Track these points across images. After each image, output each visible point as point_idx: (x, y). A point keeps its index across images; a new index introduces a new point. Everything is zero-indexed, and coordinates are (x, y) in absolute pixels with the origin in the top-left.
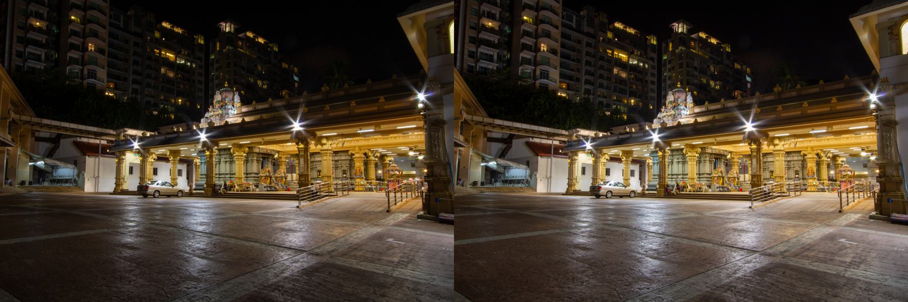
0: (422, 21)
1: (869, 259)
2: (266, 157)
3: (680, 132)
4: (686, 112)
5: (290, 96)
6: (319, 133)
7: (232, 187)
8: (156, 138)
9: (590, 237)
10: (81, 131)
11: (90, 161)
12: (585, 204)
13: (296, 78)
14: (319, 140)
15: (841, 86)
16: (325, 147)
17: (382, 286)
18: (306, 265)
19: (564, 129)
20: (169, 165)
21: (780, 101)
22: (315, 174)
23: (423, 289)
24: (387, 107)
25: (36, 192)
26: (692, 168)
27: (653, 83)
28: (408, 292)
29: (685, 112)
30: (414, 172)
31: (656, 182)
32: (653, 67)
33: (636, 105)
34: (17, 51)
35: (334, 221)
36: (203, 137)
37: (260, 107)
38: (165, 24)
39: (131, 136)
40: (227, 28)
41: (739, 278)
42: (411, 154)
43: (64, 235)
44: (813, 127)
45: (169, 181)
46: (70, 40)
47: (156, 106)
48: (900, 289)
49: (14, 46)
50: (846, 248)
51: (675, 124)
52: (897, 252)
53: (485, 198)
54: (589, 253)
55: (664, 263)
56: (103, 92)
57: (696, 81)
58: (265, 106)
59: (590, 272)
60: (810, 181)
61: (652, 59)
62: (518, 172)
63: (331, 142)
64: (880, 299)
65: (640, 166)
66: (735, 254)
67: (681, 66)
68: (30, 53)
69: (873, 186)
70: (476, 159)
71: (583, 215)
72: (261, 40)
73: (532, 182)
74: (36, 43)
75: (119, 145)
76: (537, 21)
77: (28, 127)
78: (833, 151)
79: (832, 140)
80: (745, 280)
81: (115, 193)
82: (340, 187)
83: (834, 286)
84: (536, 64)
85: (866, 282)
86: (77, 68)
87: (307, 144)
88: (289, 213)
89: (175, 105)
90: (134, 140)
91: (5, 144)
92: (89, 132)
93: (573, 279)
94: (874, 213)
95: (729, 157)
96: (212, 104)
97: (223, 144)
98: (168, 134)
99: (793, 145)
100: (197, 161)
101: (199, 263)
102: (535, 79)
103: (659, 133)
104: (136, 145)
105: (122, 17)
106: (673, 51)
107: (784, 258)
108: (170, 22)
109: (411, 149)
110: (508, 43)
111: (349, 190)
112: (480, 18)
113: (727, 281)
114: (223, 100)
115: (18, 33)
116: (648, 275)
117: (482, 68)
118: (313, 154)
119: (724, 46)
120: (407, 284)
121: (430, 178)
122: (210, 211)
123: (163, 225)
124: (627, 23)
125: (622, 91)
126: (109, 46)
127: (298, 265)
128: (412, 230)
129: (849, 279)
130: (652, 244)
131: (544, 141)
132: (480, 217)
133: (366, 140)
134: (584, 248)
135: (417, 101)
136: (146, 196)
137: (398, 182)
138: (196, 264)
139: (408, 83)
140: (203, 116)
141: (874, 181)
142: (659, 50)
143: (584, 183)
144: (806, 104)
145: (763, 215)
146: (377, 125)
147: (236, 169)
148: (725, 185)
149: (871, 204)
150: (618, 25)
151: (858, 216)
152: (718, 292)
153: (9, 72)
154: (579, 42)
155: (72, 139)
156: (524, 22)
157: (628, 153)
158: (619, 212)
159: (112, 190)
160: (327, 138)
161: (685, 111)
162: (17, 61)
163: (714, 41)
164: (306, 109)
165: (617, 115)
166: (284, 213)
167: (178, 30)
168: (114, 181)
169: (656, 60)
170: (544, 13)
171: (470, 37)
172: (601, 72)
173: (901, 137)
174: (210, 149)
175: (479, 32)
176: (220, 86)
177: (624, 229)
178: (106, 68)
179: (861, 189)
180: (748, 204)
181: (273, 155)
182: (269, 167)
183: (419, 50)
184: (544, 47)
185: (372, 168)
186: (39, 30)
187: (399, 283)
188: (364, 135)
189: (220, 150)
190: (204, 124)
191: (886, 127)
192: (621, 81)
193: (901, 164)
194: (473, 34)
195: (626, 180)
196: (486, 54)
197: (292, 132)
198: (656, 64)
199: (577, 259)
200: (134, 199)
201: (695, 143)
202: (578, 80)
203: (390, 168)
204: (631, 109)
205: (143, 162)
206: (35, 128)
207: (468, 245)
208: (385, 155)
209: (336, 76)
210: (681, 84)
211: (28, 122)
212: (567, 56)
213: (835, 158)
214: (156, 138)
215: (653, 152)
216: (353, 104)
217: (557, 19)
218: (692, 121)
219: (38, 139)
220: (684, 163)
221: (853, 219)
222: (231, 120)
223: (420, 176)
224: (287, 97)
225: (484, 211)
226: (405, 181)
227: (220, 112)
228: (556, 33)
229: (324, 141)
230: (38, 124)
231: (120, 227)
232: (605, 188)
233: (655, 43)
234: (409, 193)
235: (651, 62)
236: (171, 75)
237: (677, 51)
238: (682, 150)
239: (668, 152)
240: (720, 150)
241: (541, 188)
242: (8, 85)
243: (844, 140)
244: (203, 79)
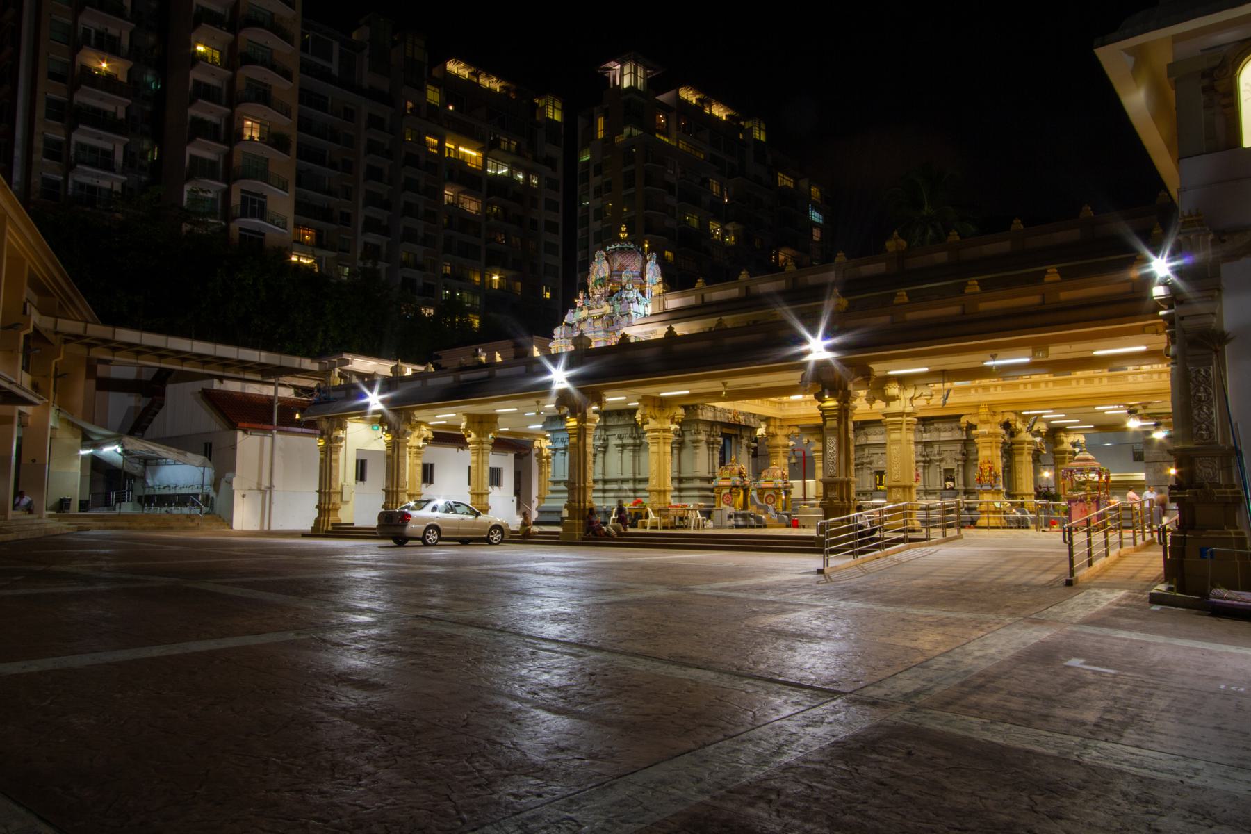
0: (1163, 58)
1: (1149, 716)
2: (732, 434)
3: (624, 363)
5: (798, 265)
6: (878, 369)
7: (639, 515)
8: (431, 382)
9: (380, 651)
10: (224, 363)
11: (248, 445)
13: (815, 216)
14: (878, 387)
16: (896, 407)
17: (1053, 789)
18: (842, 733)
20: (467, 457)
22: (868, 481)
24: (1066, 295)
25: (98, 530)
27: (552, 227)
28: (1125, 807)
29: (641, 309)
30: (1141, 476)
34: (47, 141)
35: (920, 611)
36: (559, 377)
37: (717, 295)
38: (454, 67)
40: (626, 76)
42: (1133, 424)
43: (176, 650)
45: (467, 500)
46: (192, 112)
47: (429, 292)
49: (39, 128)
52: (1225, 695)
55: (581, 725)
56: (284, 253)
58: (730, 292)
59: (378, 750)
60: (987, 498)
61: (550, 162)
62: (181, 473)
63: (912, 391)
64: (1179, 824)
65: (518, 458)
66: (778, 701)
68: (82, 147)
70: (67, 438)
72: (719, 112)
74: (99, 119)
75: (327, 401)
76: (234, 58)
77: (78, 350)
79: (1046, 386)
80: (807, 773)
82: (935, 516)
85: (1142, 780)
86: (211, 189)
87: (845, 398)
88: (797, 587)
89: (484, 289)
90: (370, 386)
91: (11, 398)
92: (245, 366)
93: (334, 767)
95: (761, 431)
96: (585, 287)
97: (614, 398)
98: (464, 369)
99: (937, 400)
100: (544, 444)
101: (547, 728)
104: (375, 400)
105: (336, 46)
108: (468, 61)
109: (1132, 412)
111: (962, 525)
112: (76, 49)
113: (757, 773)
114: (614, 277)
115: (50, 90)
118: (862, 426)
120: (1122, 785)
121: (1186, 492)
122: (579, 582)
123: (450, 622)
124: (480, 64)
126: (300, 129)
127: (820, 731)
128: (1135, 636)
133: (1009, 387)
135: (1148, 280)
136: (401, 540)
137: (1097, 502)
139: (1124, 229)
140: (558, 321)
142: (570, 136)
143: (361, 506)
146: (1037, 346)
147: (651, 466)
148: (752, 510)
152: (731, 806)
153: (25, 198)
154: (349, 115)
155: (198, 385)
157: (482, 423)
159: (308, 525)
160: (902, 381)
162: (48, 170)
166: (781, 588)
167: (492, 84)
168: (314, 499)
169: (560, 166)
171: (51, 103)
174: (577, 410)
176: (606, 238)
177: (471, 632)
178: (292, 188)
181: (753, 429)
182: (742, 462)
183: (1154, 139)
184: (251, 130)
185: (1025, 464)
186: (108, 82)
187: (1099, 780)
188: (1003, 371)
189: (605, 414)
190: (561, 342)
191: (1196, 349)
193: (1239, 453)
194: (58, 92)
197: (803, 366)
199: (345, 713)
200: (371, 549)
201: (668, 393)
202: (346, 219)
203: (1074, 465)
205: (395, 448)
206: (96, 353)
208: (1062, 429)
209: (927, 210)
211: (78, 337)
214: (431, 382)
215: (551, 419)
216: (973, 286)
219: (106, 385)
220: (638, 448)
222: (636, 332)
223: (1157, 487)
224: (791, 267)
226: (1116, 501)
229: (893, 390)
230: (105, 342)
231: (332, 628)
233: (557, 117)
234: (1127, 534)
236: (472, 206)
240: (736, 414)
242: (21, 237)
244: (559, 218)
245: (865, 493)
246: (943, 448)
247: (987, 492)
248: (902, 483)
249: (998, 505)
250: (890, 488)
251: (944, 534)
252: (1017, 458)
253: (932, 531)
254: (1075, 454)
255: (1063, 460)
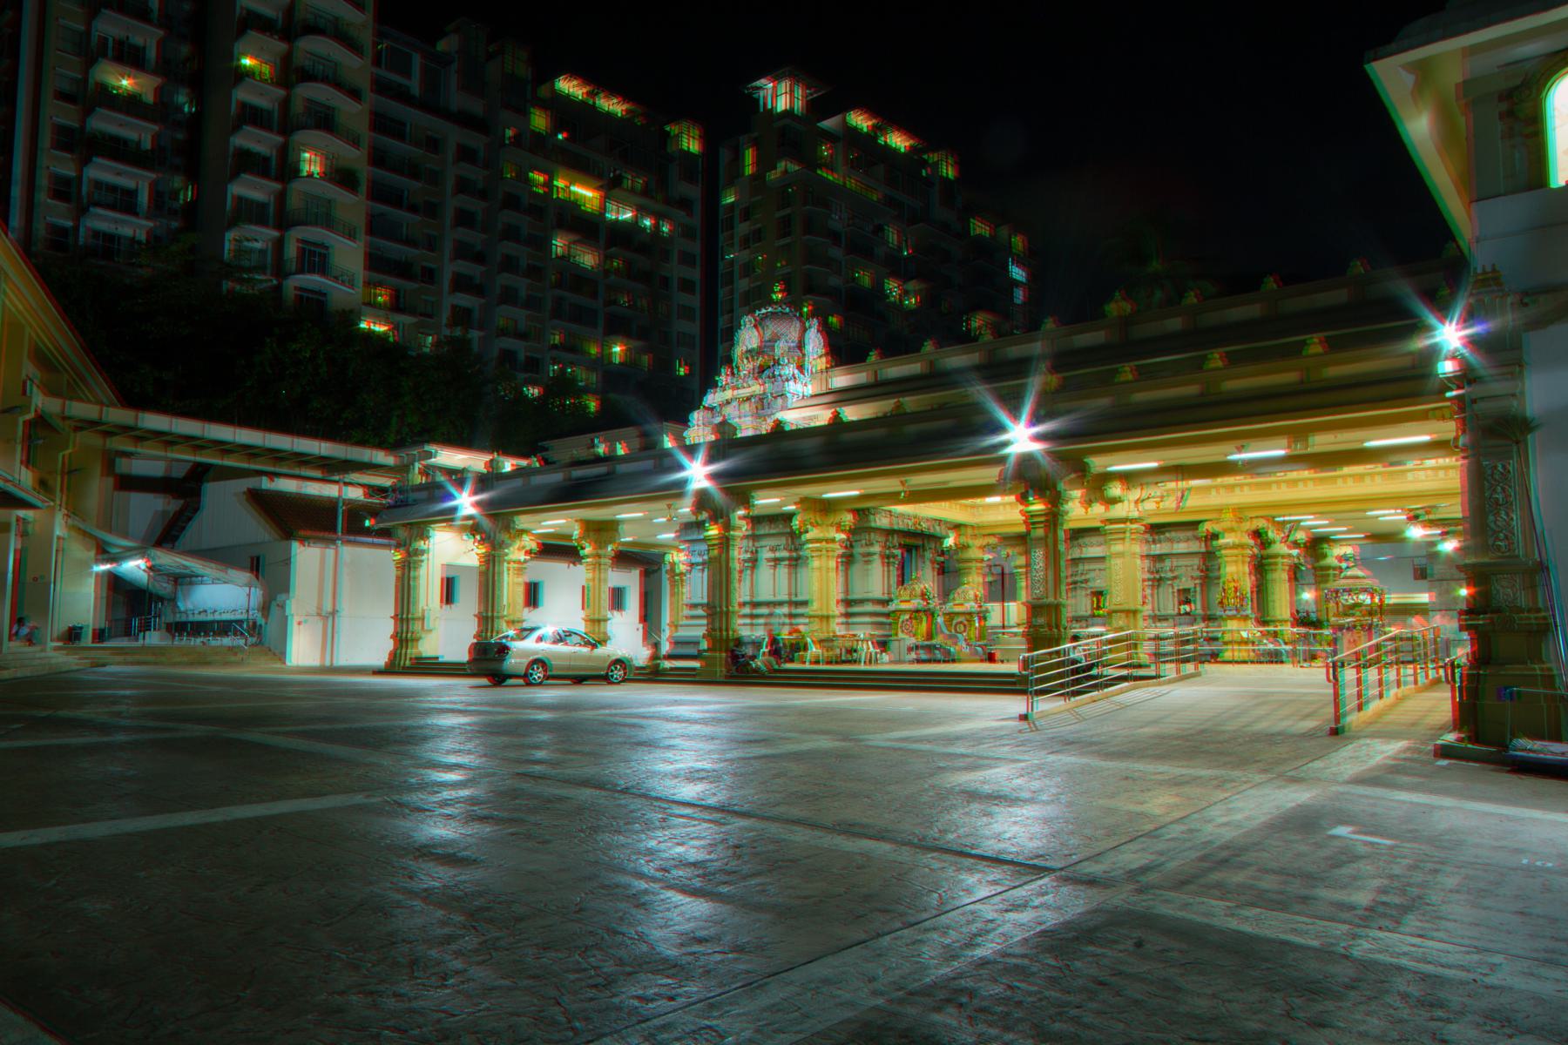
0: (1452, 76)
1: (1434, 898)
3: (781, 456)
4: (800, 387)
8: (537, 480)
10: (276, 456)
12: (452, 706)
14: (1097, 486)
15: (1339, 296)
16: (1118, 511)
19: (381, 445)
21: (1126, 348)
23: (1455, 999)
26: (822, 581)
31: (697, 630)
32: (687, 233)
33: (629, 364)
39: (449, 472)
41: (984, 963)
42: (1416, 533)
44: (1242, 439)
45: (581, 627)
48: (1538, 1000)
50: (1356, 858)
51: (765, 428)
52: (1529, 871)
53: (108, 685)
54: (466, 876)
55: (724, 909)
57: (834, 281)
59: (470, 941)
60: (1232, 625)
62: (222, 594)
64: (1472, 1033)
66: (971, 880)
67: (785, 227)
69: (1448, 645)
70: (79, 550)
71: (448, 744)
73: (270, 630)
74: (118, 150)
76: (289, 73)
78: (1309, 521)
79: (1305, 485)
81: (391, 669)
83: (1314, 989)
84: (284, 220)
86: (260, 238)
88: (995, 737)
92: (302, 460)
94: (1450, 737)
95: (949, 542)
102: (280, 271)
103: (711, 459)
104: (466, 502)
105: (417, 60)
106: (758, 177)
107: (1140, 891)
109: (1413, 518)
110: (188, 147)
111: (1201, 659)
112: (90, 61)
113: (945, 970)
115: (58, 114)
116: (672, 953)
117: (96, 234)
118: (1078, 534)
119: (932, 158)
120: (1400, 984)
124: (598, 80)
125: (582, 316)
127: (1025, 917)
129: (1365, 965)
130: (685, 843)
131: (314, 489)
132: (90, 750)
134: (448, 856)
135: (1432, 354)
138: (674, 915)
141: (1447, 625)
142: (710, 172)
143: (448, 635)
144: (1215, 359)
145: (1066, 744)
149: (1440, 705)
150: (569, 87)
151: (1394, 747)
152: (911, 1011)
153: (26, 247)
154: (433, 144)
156: (242, 75)
157: (601, 531)
158: (572, 732)
159: (381, 660)
160: (1127, 478)
161: (794, 382)
162: (55, 214)
163: (898, 141)
164: (1054, 380)
165: (566, 395)
168: (389, 627)
169: (697, 208)
170: (313, 47)
172: (509, 248)
173: (1542, 473)
174: (719, 515)
175: (88, 111)
177: (586, 793)
178: (362, 238)
179: (1407, 653)
180: (1016, 705)
182: (926, 580)
183: (1441, 177)
184: (311, 163)
186: (130, 104)
189: (756, 521)
191: (1495, 438)
192: (577, 279)
195: (596, 621)
196: (113, 189)
198: (696, 221)
199: (427, 896)
200: (460, 690)
202: (429, 276)
203: (1341, 583)
204: (613, 378)
207: (47, 846)
210: (787, 290)
211: (92, 424)
212: (393, 191)
213: (1316, 545)
214: (537, 480)
217: (354, 66)
218: (822, 417)
220: (796, 562)
221: (1377, 759)
223: (1445, 609)
225: (104, 728)
227: (756, 388)
228: (352, 112)
230: (125, 429)
231: (411, 789)
232: (524, 649)
235: (681, 215)
237: (772, 176)
238: (789, 517)
239: (742, 528)
241: (302, 650)
243: (1349, 482)
244: (695, 274)
245: (1078, 619)
246: (1182, 562)
247: (1231, 618)
248: (1126, 607)
249: (1244, 634)
250: (1110, 613)
251: (1178, 671)
252: (1270, 576)
253: (1163, 666)
254: (1341, 570)
255: (1325, 579)
